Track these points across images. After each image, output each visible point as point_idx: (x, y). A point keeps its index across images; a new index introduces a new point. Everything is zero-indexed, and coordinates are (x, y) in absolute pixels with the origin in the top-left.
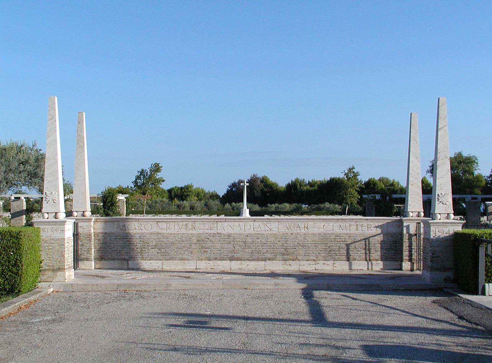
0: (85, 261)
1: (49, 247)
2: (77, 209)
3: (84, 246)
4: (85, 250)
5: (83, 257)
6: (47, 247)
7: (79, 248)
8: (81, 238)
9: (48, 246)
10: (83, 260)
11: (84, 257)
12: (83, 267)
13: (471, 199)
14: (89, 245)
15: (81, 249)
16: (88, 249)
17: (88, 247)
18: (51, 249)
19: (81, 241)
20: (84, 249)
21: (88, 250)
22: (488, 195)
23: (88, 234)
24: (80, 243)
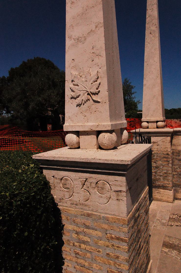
0: (162, 189)
1: (81, 236)
2: (148, 119)
3: (159, 169)
4: (161, 174)
5: (158, 183)
6: (74, 236)
7: (153, 171)
8: (155, 157)
9: (77, 233)
10: (159, 187)
11: (159, 183)
12: (159, 197)
13: (160, 117)
14: (166, 168)
15: (156, 173)
16: (165, 173)
17: (165, 171)
18: (84, 242)
19: (155, 162)
20: (160, 172)
21: (165, 175)
22: (119, 123)
23: (165, 153)
24: (154, 165)
